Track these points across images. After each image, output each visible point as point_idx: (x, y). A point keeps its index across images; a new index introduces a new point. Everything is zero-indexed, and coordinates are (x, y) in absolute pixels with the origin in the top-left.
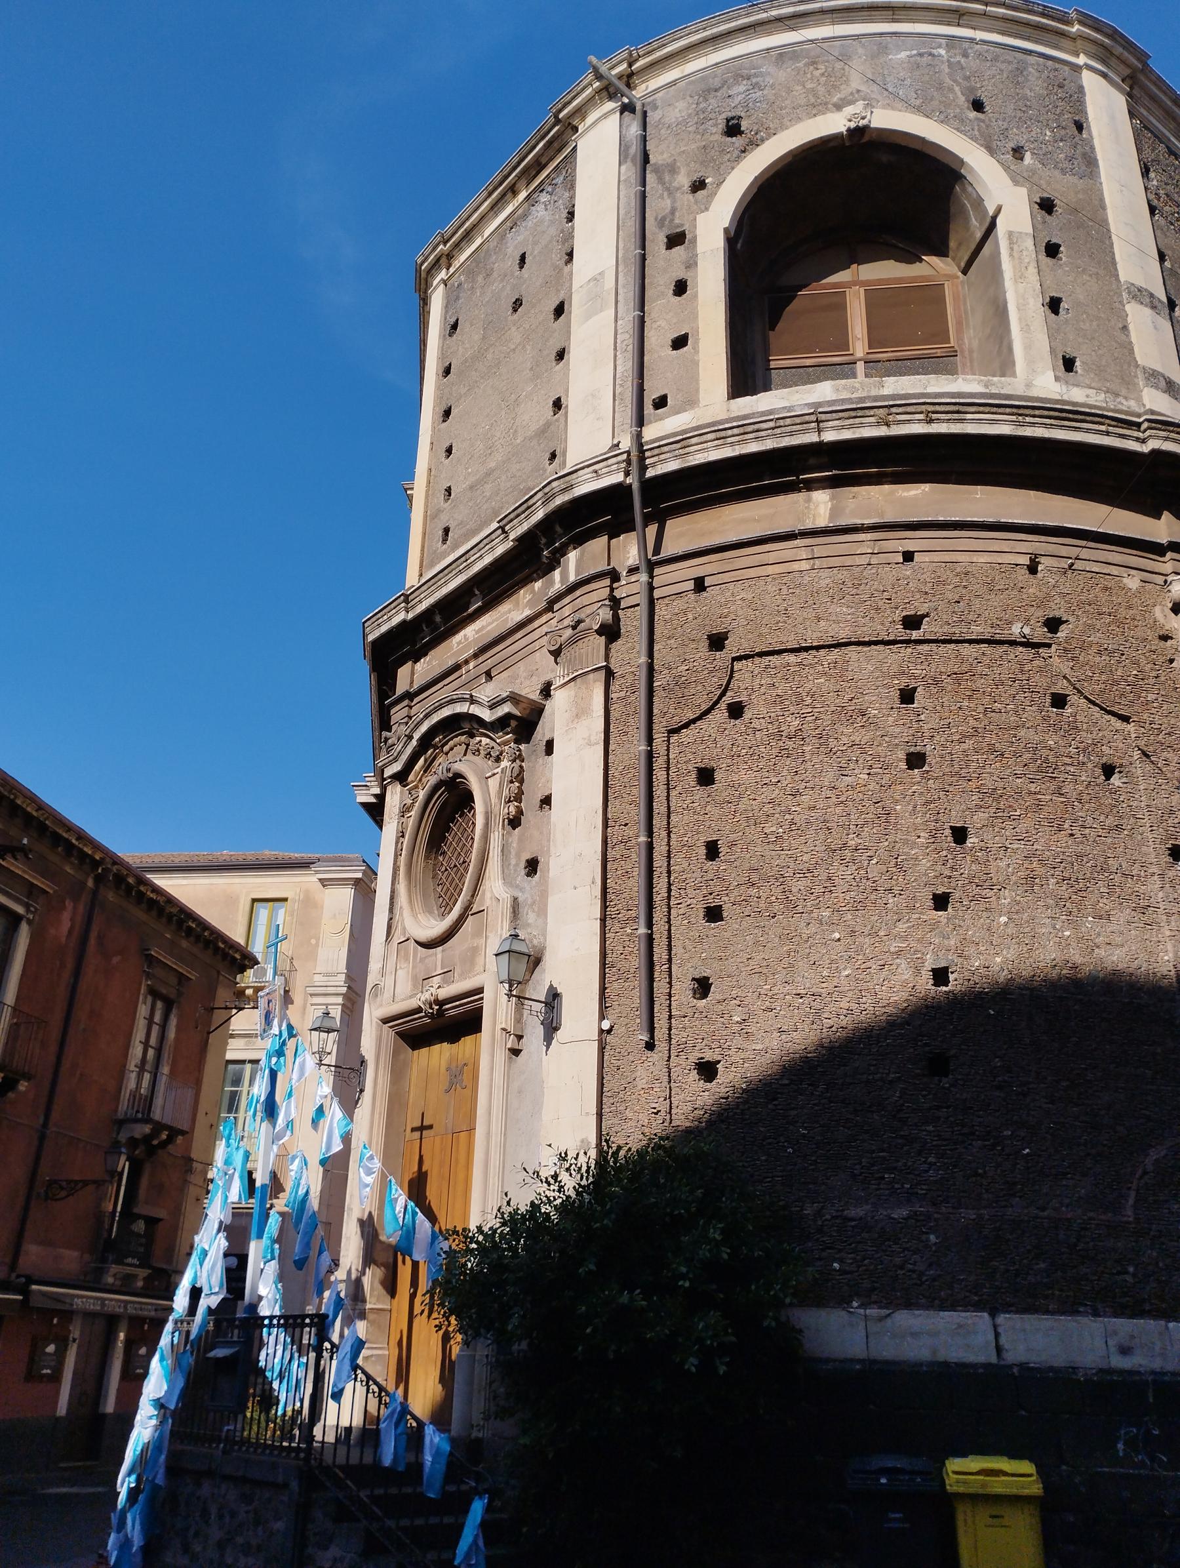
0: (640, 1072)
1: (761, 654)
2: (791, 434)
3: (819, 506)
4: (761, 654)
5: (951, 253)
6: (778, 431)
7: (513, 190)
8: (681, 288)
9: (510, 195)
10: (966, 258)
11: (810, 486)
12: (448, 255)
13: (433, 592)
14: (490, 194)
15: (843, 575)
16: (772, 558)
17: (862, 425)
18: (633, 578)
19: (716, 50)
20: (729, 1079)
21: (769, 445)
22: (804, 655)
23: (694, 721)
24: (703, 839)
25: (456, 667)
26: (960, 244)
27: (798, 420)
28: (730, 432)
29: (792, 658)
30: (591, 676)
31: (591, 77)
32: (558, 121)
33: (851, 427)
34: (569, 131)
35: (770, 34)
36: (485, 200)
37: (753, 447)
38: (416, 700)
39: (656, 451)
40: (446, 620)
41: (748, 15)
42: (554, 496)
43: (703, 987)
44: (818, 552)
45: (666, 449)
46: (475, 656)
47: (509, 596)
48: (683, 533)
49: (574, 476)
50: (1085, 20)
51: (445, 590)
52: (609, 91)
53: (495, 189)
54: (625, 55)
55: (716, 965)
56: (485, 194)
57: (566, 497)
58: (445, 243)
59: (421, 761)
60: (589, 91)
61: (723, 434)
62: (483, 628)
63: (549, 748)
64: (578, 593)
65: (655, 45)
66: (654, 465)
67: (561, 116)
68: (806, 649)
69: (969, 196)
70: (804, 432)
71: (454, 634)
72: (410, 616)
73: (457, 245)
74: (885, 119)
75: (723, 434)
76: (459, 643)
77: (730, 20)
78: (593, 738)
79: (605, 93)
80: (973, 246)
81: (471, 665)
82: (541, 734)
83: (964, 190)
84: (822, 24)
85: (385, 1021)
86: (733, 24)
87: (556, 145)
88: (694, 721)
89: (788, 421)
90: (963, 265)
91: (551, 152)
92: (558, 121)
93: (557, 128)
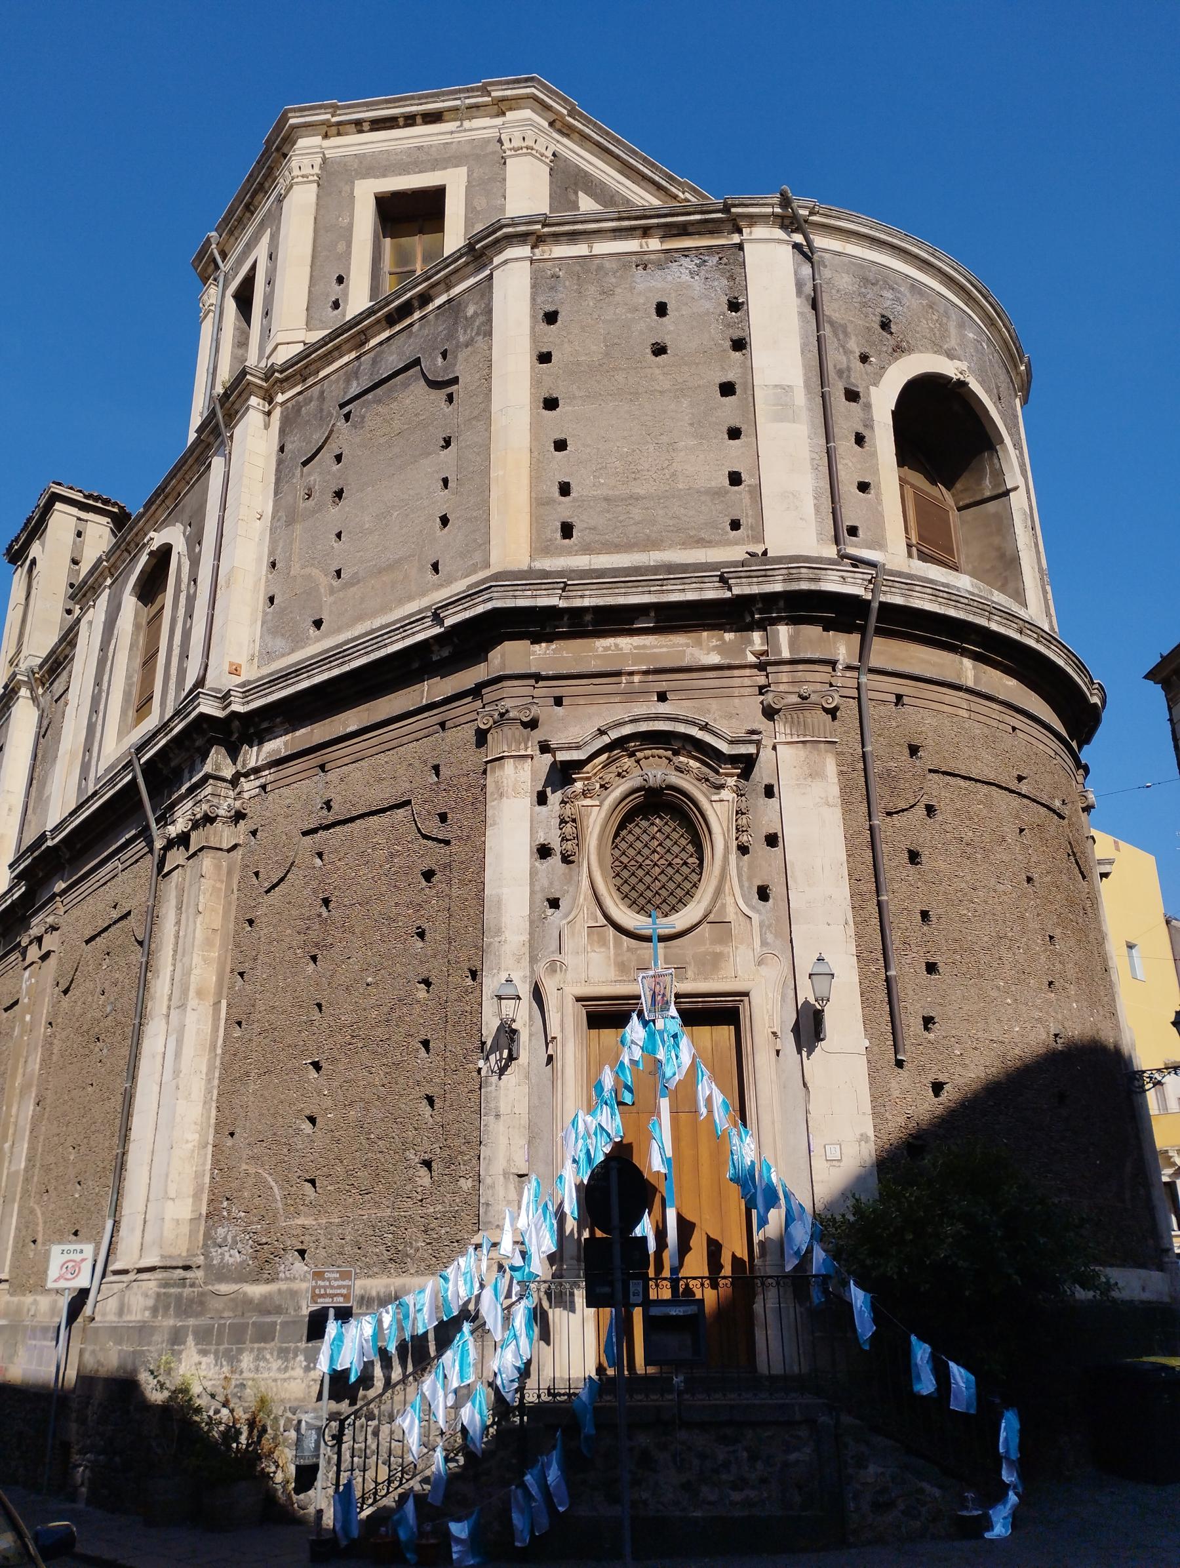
0: (894, 1084)
1: (945, 773)
2: (975, 614)
3: (967, 670)
4: (945, 773)
5: (953, 490)
6: (969, 608)
7: (646, 232)
8: (860, 440)
9: (639, 232)
10: (967, 501)
11: (964, 653)
12: (539, 237)
13: (603, 595)
14: (620, 219)
15: (986, 730)
16: (947, 699)
17: (1009, 627)
18: (848, 674)
19: (870, 248)
20: (949, 1095)
21: (961, 615)
22: (968, 783)
23: (903, 811)
24: (919, 907)
25: (618, 674)
26: (966, 490)
27: (981, 606)
28: (941, 594)
29: (962, 783)
30: (822, 745)
31: (776, 201)
32: (726, 209)
33: (1004, 625)
34: (730, 226)
35: (906, 262)
36: (612, 220)
37: (952, 613)
38: (541, 684)
39: (890, 584)
40: (595, 623)
41: (901, 239)
42: (799, 579)
43: (928, 1021)
44: (974, 707)
45: (897, 585)
46: (646, 673)
47: (686, 632)
48: (888, 652)
49: (823, 572)
50: (1028, 367)
51: (622, 600)
52: (790, 223)
53: (629, 219)
54: (811, 205)
55: (938, 1008)
56: (616, 215)
57: (813, 586)
58: (544, 225)
59: (605, 756)
60: (769, 210)
61: (937, 593)
62: (644, 647)
63: (769, 792)
64: (800, 667)
65: (834, 213)
66: (885, 593)
67: (733, 210)
68: (970, 779)
69: (992, 465)
70: (982, 616)
71: (599, 637)
72: (562, 604)
73: (555, 235)
74: (975, 386)
75: (937, 593)
76: (607, 649)
77: (890, 235)
78: (830, 800)
79: (779, 220)
80: (978, 498)
81: (636, 678)
82: (762, 774)
83: (991, 459)
84: (933, 277)
85: (579, 999)
86: (890, 239)
87: (710, 225)
88: (903, 811)
89: (976, 604)
90: (961, 504)
91: (702, 228)
92: (726, 209)
93: (720, 215)
